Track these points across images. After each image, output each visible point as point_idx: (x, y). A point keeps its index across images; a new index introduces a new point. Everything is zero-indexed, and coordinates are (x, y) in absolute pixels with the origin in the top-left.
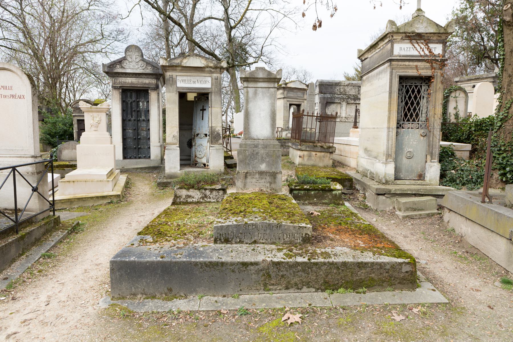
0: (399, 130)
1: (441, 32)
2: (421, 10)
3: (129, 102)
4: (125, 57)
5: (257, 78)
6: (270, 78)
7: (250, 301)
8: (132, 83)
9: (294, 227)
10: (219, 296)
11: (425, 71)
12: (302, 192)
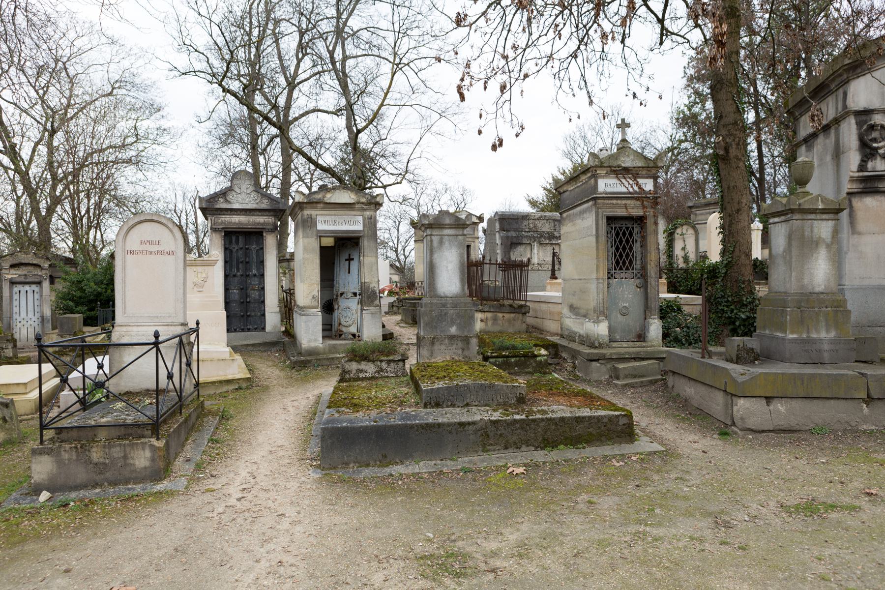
0: (611, 281)
1: (650, 166)
2: (627, 141)
3: (234, 250)
4: (231, 187)
5: (443, 224)
6: (458, 225)
7: (470, 462)
8: (240, 223)
9: (507, 386)
10: (436, 460)
11: (635, 210)
12: (500, 360)
